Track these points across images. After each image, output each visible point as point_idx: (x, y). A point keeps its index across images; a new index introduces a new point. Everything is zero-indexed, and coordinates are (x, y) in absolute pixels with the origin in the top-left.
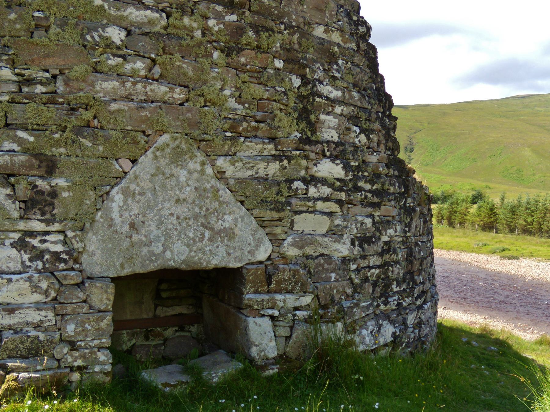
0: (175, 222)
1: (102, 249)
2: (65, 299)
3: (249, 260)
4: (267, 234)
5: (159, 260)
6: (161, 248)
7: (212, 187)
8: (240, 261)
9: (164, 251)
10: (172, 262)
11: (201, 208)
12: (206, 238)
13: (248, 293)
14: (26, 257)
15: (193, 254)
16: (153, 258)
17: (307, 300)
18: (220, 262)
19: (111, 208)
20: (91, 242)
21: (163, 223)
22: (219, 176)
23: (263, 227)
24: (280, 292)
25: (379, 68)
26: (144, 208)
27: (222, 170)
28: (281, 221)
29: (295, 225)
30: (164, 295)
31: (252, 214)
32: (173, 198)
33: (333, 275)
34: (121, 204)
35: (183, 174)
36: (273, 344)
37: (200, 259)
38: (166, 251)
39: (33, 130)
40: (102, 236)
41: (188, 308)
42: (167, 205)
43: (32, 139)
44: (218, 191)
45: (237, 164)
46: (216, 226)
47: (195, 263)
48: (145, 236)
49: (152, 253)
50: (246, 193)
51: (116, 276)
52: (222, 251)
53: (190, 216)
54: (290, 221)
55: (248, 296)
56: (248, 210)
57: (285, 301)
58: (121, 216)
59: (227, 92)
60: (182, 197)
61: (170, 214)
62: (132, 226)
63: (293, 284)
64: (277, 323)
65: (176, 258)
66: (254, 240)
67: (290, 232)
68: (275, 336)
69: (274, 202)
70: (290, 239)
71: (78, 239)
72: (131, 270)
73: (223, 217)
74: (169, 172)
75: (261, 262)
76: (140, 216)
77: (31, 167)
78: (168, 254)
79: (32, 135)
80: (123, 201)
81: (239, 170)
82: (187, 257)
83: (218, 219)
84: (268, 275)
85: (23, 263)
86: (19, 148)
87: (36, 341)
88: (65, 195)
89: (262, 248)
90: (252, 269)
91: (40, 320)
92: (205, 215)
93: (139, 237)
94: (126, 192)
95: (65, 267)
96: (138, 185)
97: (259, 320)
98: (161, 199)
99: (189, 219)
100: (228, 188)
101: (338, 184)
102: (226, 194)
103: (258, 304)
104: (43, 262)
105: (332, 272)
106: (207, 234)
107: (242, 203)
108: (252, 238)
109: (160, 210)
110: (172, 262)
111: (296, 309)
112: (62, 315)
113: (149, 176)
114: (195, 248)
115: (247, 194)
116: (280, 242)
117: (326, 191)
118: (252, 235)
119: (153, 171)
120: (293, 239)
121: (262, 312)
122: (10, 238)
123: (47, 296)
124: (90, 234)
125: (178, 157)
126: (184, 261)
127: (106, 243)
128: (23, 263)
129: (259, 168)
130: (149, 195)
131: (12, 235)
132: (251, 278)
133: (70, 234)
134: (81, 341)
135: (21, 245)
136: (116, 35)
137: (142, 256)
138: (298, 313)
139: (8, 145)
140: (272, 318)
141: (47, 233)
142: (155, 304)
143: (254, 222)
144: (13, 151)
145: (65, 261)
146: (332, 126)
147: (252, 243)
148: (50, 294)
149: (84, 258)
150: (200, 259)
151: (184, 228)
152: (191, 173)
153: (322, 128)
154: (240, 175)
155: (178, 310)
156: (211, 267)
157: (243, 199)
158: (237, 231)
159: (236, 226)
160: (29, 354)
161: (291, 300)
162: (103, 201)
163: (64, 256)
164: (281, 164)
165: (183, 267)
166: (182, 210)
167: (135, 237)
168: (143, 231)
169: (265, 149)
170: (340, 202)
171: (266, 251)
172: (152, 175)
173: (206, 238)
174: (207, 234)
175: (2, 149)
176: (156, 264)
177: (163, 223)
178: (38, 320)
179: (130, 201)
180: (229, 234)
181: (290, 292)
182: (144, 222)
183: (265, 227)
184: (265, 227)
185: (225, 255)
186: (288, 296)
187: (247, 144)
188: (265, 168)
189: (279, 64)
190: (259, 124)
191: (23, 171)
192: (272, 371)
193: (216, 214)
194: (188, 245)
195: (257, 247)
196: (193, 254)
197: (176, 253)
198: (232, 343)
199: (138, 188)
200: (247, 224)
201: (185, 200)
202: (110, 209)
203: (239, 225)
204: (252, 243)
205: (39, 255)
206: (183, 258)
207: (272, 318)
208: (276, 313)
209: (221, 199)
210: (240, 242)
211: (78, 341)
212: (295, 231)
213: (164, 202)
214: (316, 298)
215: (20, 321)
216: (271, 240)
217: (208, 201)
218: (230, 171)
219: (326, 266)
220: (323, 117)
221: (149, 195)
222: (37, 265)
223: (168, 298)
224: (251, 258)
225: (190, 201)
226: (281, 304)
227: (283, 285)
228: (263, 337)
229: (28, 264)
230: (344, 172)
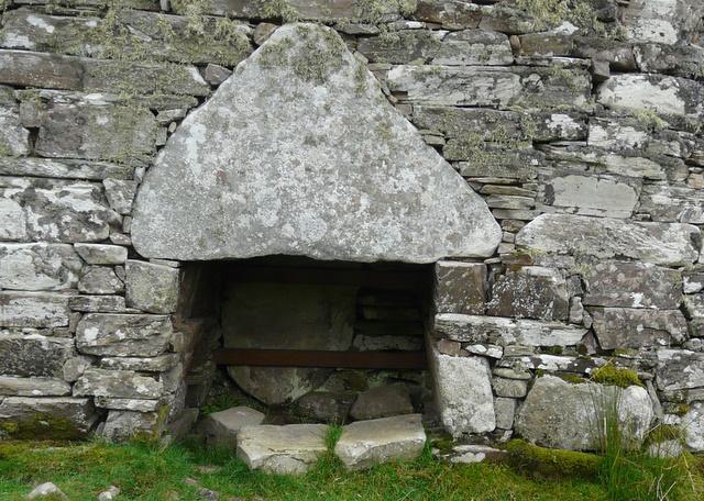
0: (303, 175)
1: (166, 212)
2: (87, 286)
3: (450, 252)
4: (491, 209)
5: (269, 238)
6: (274, 218)
7: (378, 118)
8: (430, 251)
9: (281, 225)
10: (295, 243)
11: (353, 154)
12: (363, 208)
13: (444, 311)
14: (34, 217)
15: (335, 232)
16: (260, 235)
18: (390, 250)
19: (185, 147)
20: (147, 201)
21: (279, 176)
22: (394, 99)
23: (484, 195)
24: (510, 314)
26: (245, 149)
27: (400, 89)
28: (521, 187)
29: (557, 197)
30: (369, 314)
31: (458, 170)
32: (300, 133)
33: (638, 297)
34: (203, 140)
35: (320, 93)
36: (489, 407)
37: (348, 242)
38: (284, 223)
39: (56, 14)
40: (166, 192)
41: (410, 341)
42: (287, 145)
43: (51, 29)
44: (388, 126)
45: (428, 80)
46: (383, 187)
47: (339, 249)
48: (246, 197)
49: (258, 226)
51: (191, 259)
52: (395, 230)
53: (331, 167)
54: (542, 187)
55: (445, 317)
56: (450, 162)
57: (517, 333)
58: (200, 161)
60: (318, 132)
61: (293, 162)
62: (222, 177)
63: (537, 302)
64: (499, 371)
65: (303, 238)
66: (462, 216)
67: (541, 207)
68: (494, 392)
70: (538, 221)
71: (120, 194)
72: (218, 251)
73: (397, 171)
74: (294, 89)
75: (480, 259)
76: (237, 162)
77: (49, 74)
78: (288, 230)
79: (51, 23)
80: (206, 135)
81: (436, 90)
82: (324, 237)
83: (388, 175)
85: (29, 226)
86: (32, 44)
87: (37, 350)
88: (102, 121)
89: (479, 233)
90: (449, 268)
91: (46, 318)
92: (362, 168)
93: (235, 196)
94: (214, 122)
95: (95, 238)
96: (234, 109)
97: (462, 362)
98: (277, 136)
99: (330, 172)
100: (412, 122)
101: (663, 124)
102: (404, 131)
103: (460, 333)
104: (59, 226)
105: (636, 291)
106: (364, 202)
107: (439, 148)
108: (457, 214)
109: (274, 153)
110: (295, 243)
111: (545, 350)
112: (81, 312)
113: (254, 95)
114: (340, 223)
115: (449, 133)
116: (518, 224)
117: (634, 137)
118: (458, 209)
119: (262, 87)
120: (546, 220)
121: (469, 348)
122: (14, 187)
123: (62, 280)
124: (145, 188)
125: (312, 68)
126: (317, 245)
127: (174, 204)
128: (29, 226)
129: (478, 88)
130: (253, 126)
131: (16, 181)
132: (448, 283)
133: (108, 184)
134: (110, 356)
135: (25, 200)
137: (239, 230)
138: (544, 357)
139: (13, 39)
140: (492, 362)
141: (72, 180)
142: (355, 330)
143: (463, 184)
144: (23, 48)
145: (96, 227)
146: (662, 12)
147: (457, 221)
148: (67, 277)
149: (133, 225)
150: (348, 242)
151: (319, 187)
153: (638, 17)
155: (387, 342)
156: (371, 258)
157: (441, 141)
158: (425, 198)
159: (424, 189)
160: (30, 370)
161: (532, 333)
162: (169, 134)
163: (95, 219)
164: (524, 80)
165: (317, 254)
166: (320, 156)
167: (227, 197)
168: (242, 188)
169: (490, 53)
171: (487, 239)
172: (261, 95)
173: (363, 208)
174: (364, 202)
175: (5, 44)
176: (264, 245)
177: (279, 176)
178: (42, 316)
179: (218, 135)
181: (534, 317)
182: (243, 173)
183: (488, 195)
184: (488, 195)
185: (399, 239)
186: (525, 323)
187: (452, 42)
188: (490, 88)
191: (35, 80)
192: (472, 455)
193: (384, 166)
194: (327, 218)
195: (468, 229)
196: (335, 232)
197: (303, 228)
199: (233, 115)
200: (448, 187)
201: (322, 139)
202: (183, 149)
203: (431, 188)
204: (457, 221)
205: (54, 214)
206: (318, 238)
207: (492, 362)
208: (495, 352)
209: (394, 140)
211: (104, 356)
212: (557, 207)
213: (282, 140)
214: (590, 335)
215: (18, 316)
216: (499, 221)
217: (368, 142)
218: (415, 92)
219: (621, 277)
221: (253, 126)
222: (50, 231)
223: (373, 320)
224: (452, 249)
225: (333, 139)
226: (509, 338)
227: (516, 304)
229: (37, 228)
230: (683, 103)
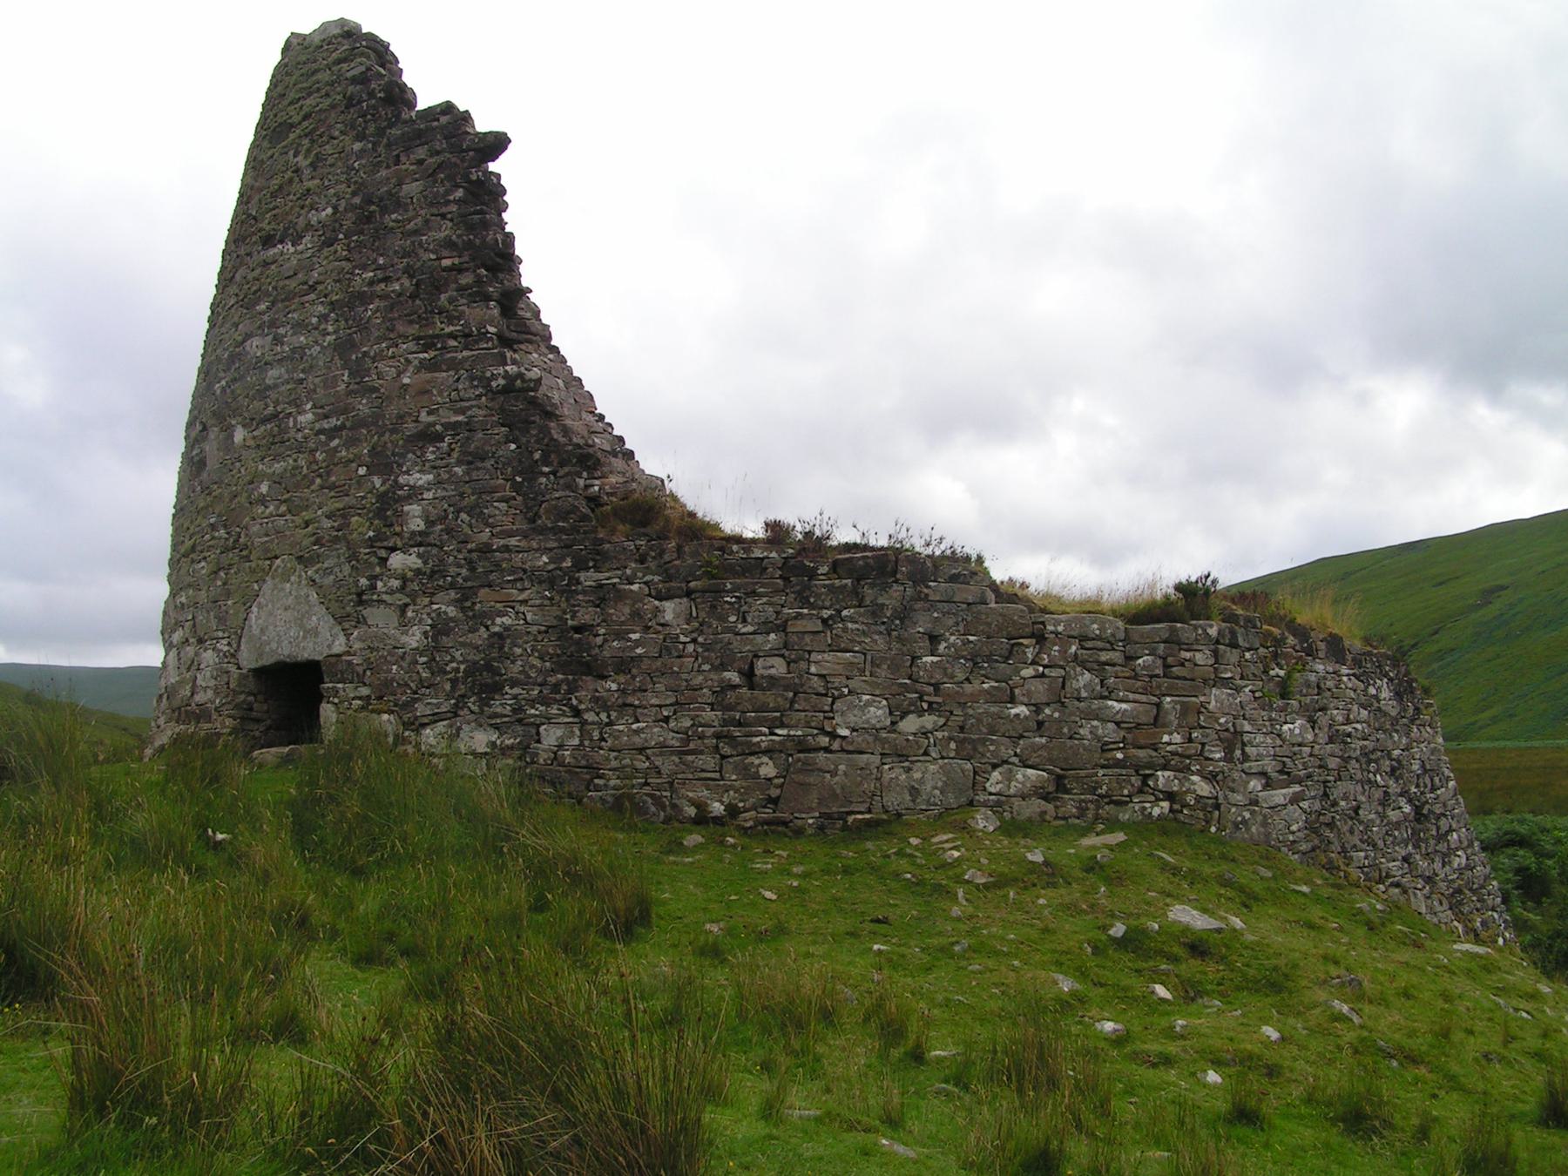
69: (351, 607)
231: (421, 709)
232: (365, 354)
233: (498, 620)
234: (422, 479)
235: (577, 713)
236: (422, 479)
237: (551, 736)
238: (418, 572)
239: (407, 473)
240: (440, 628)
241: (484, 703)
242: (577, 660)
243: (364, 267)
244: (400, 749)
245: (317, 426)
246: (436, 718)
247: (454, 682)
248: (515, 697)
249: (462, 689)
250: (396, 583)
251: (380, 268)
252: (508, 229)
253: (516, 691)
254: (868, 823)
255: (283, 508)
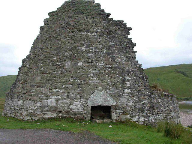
14: (80, 103)
17: (122, 111)
25: (102, 7)
50: (111, 95)
59: (108, 81)
69: (116, 97)
84: (116, 107)
102: (108, 95)
136: (92, 75)
152: (103, 93)
154: (110, 93)
161: (119, 111)
166: (102, 97)
170: (130, 96)
180: (109, 101)
189: (117, 75)
190: (114, 85)
198: (110, 117)
205: (82, 103)
207: (116, 114)
210: (110, 102)
220: (127, 83)
228: (114, 116)
231: (133, 114)
232: (114, 56)
233: (143, 101)
234: (129, 78)
235: (153, 114)
236: (129, 78)
237: (151, 118)
238: (131, 93)
239: (126, 77)
240: (135, 102)
241: (143, 113)
242: (152, 108)
243: (112, 42)
244: (130, 121)
245: (105, 66)
246: (136, 116)
247: (138, 110)
248: (146, 112)
249: (139, 111)
250: (127, 94)
251: (114, 43)
252: (32, 46)
253: (146, 112)
254: (65, 117)
255: (98, 79)
